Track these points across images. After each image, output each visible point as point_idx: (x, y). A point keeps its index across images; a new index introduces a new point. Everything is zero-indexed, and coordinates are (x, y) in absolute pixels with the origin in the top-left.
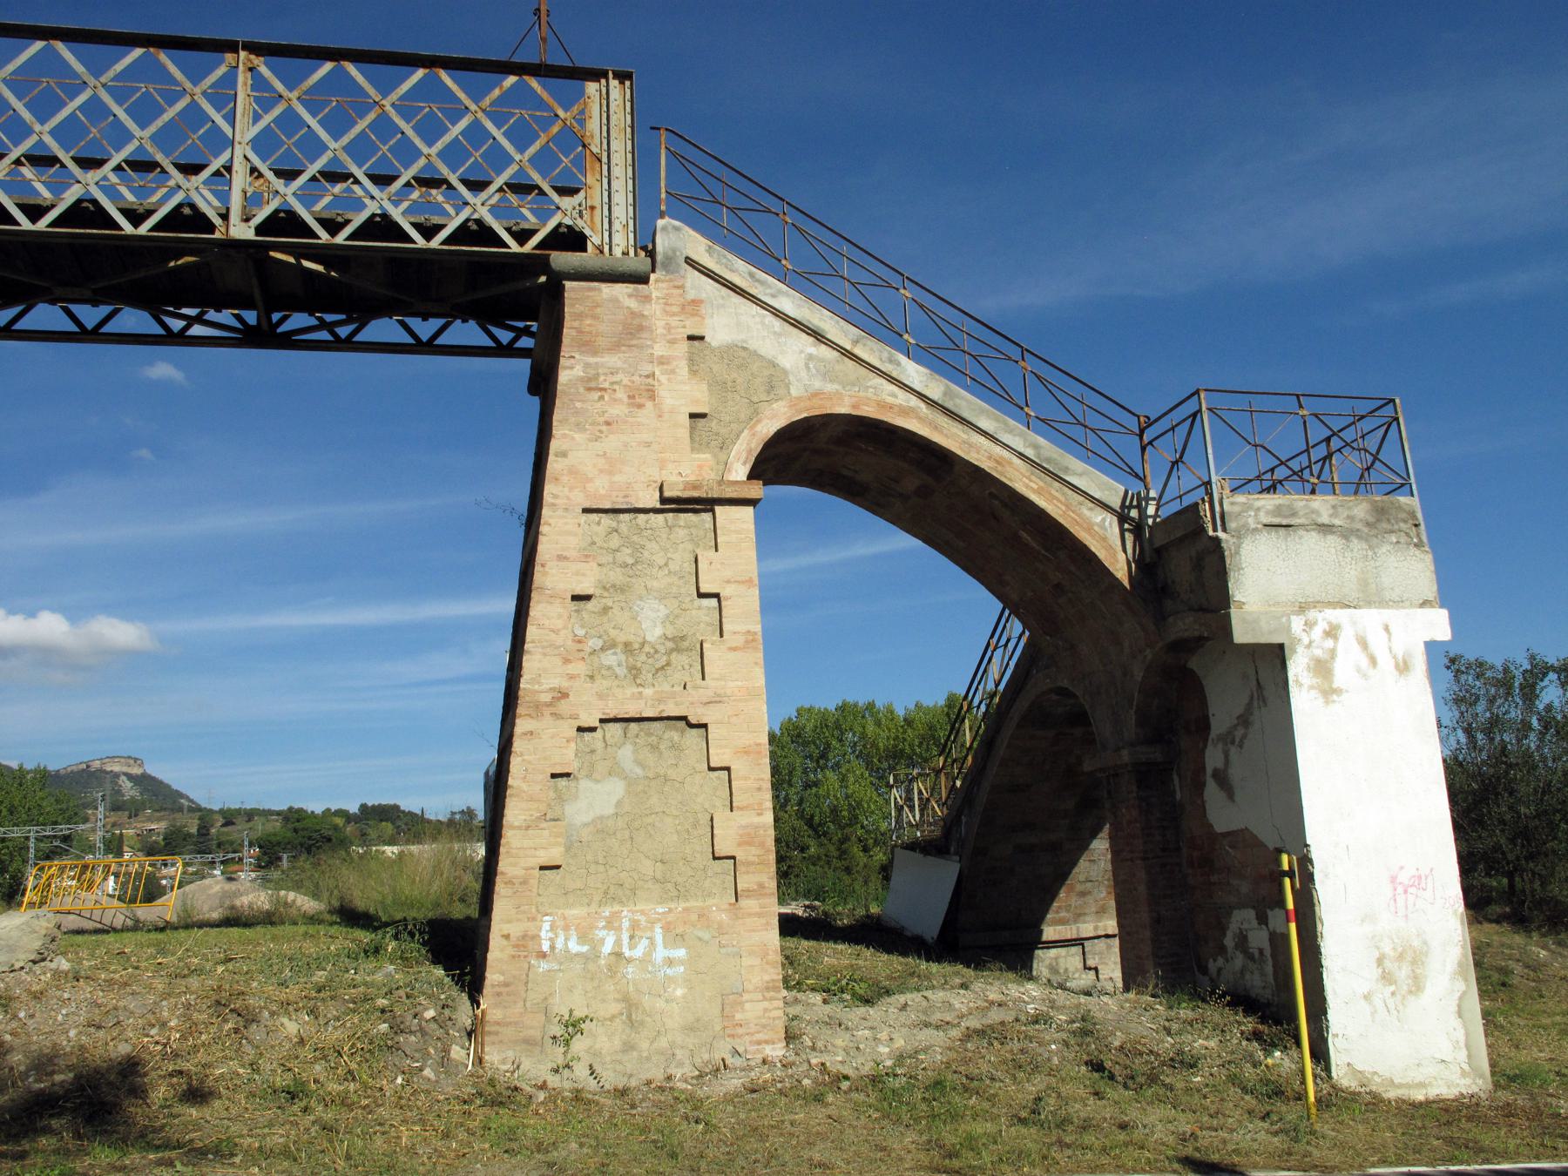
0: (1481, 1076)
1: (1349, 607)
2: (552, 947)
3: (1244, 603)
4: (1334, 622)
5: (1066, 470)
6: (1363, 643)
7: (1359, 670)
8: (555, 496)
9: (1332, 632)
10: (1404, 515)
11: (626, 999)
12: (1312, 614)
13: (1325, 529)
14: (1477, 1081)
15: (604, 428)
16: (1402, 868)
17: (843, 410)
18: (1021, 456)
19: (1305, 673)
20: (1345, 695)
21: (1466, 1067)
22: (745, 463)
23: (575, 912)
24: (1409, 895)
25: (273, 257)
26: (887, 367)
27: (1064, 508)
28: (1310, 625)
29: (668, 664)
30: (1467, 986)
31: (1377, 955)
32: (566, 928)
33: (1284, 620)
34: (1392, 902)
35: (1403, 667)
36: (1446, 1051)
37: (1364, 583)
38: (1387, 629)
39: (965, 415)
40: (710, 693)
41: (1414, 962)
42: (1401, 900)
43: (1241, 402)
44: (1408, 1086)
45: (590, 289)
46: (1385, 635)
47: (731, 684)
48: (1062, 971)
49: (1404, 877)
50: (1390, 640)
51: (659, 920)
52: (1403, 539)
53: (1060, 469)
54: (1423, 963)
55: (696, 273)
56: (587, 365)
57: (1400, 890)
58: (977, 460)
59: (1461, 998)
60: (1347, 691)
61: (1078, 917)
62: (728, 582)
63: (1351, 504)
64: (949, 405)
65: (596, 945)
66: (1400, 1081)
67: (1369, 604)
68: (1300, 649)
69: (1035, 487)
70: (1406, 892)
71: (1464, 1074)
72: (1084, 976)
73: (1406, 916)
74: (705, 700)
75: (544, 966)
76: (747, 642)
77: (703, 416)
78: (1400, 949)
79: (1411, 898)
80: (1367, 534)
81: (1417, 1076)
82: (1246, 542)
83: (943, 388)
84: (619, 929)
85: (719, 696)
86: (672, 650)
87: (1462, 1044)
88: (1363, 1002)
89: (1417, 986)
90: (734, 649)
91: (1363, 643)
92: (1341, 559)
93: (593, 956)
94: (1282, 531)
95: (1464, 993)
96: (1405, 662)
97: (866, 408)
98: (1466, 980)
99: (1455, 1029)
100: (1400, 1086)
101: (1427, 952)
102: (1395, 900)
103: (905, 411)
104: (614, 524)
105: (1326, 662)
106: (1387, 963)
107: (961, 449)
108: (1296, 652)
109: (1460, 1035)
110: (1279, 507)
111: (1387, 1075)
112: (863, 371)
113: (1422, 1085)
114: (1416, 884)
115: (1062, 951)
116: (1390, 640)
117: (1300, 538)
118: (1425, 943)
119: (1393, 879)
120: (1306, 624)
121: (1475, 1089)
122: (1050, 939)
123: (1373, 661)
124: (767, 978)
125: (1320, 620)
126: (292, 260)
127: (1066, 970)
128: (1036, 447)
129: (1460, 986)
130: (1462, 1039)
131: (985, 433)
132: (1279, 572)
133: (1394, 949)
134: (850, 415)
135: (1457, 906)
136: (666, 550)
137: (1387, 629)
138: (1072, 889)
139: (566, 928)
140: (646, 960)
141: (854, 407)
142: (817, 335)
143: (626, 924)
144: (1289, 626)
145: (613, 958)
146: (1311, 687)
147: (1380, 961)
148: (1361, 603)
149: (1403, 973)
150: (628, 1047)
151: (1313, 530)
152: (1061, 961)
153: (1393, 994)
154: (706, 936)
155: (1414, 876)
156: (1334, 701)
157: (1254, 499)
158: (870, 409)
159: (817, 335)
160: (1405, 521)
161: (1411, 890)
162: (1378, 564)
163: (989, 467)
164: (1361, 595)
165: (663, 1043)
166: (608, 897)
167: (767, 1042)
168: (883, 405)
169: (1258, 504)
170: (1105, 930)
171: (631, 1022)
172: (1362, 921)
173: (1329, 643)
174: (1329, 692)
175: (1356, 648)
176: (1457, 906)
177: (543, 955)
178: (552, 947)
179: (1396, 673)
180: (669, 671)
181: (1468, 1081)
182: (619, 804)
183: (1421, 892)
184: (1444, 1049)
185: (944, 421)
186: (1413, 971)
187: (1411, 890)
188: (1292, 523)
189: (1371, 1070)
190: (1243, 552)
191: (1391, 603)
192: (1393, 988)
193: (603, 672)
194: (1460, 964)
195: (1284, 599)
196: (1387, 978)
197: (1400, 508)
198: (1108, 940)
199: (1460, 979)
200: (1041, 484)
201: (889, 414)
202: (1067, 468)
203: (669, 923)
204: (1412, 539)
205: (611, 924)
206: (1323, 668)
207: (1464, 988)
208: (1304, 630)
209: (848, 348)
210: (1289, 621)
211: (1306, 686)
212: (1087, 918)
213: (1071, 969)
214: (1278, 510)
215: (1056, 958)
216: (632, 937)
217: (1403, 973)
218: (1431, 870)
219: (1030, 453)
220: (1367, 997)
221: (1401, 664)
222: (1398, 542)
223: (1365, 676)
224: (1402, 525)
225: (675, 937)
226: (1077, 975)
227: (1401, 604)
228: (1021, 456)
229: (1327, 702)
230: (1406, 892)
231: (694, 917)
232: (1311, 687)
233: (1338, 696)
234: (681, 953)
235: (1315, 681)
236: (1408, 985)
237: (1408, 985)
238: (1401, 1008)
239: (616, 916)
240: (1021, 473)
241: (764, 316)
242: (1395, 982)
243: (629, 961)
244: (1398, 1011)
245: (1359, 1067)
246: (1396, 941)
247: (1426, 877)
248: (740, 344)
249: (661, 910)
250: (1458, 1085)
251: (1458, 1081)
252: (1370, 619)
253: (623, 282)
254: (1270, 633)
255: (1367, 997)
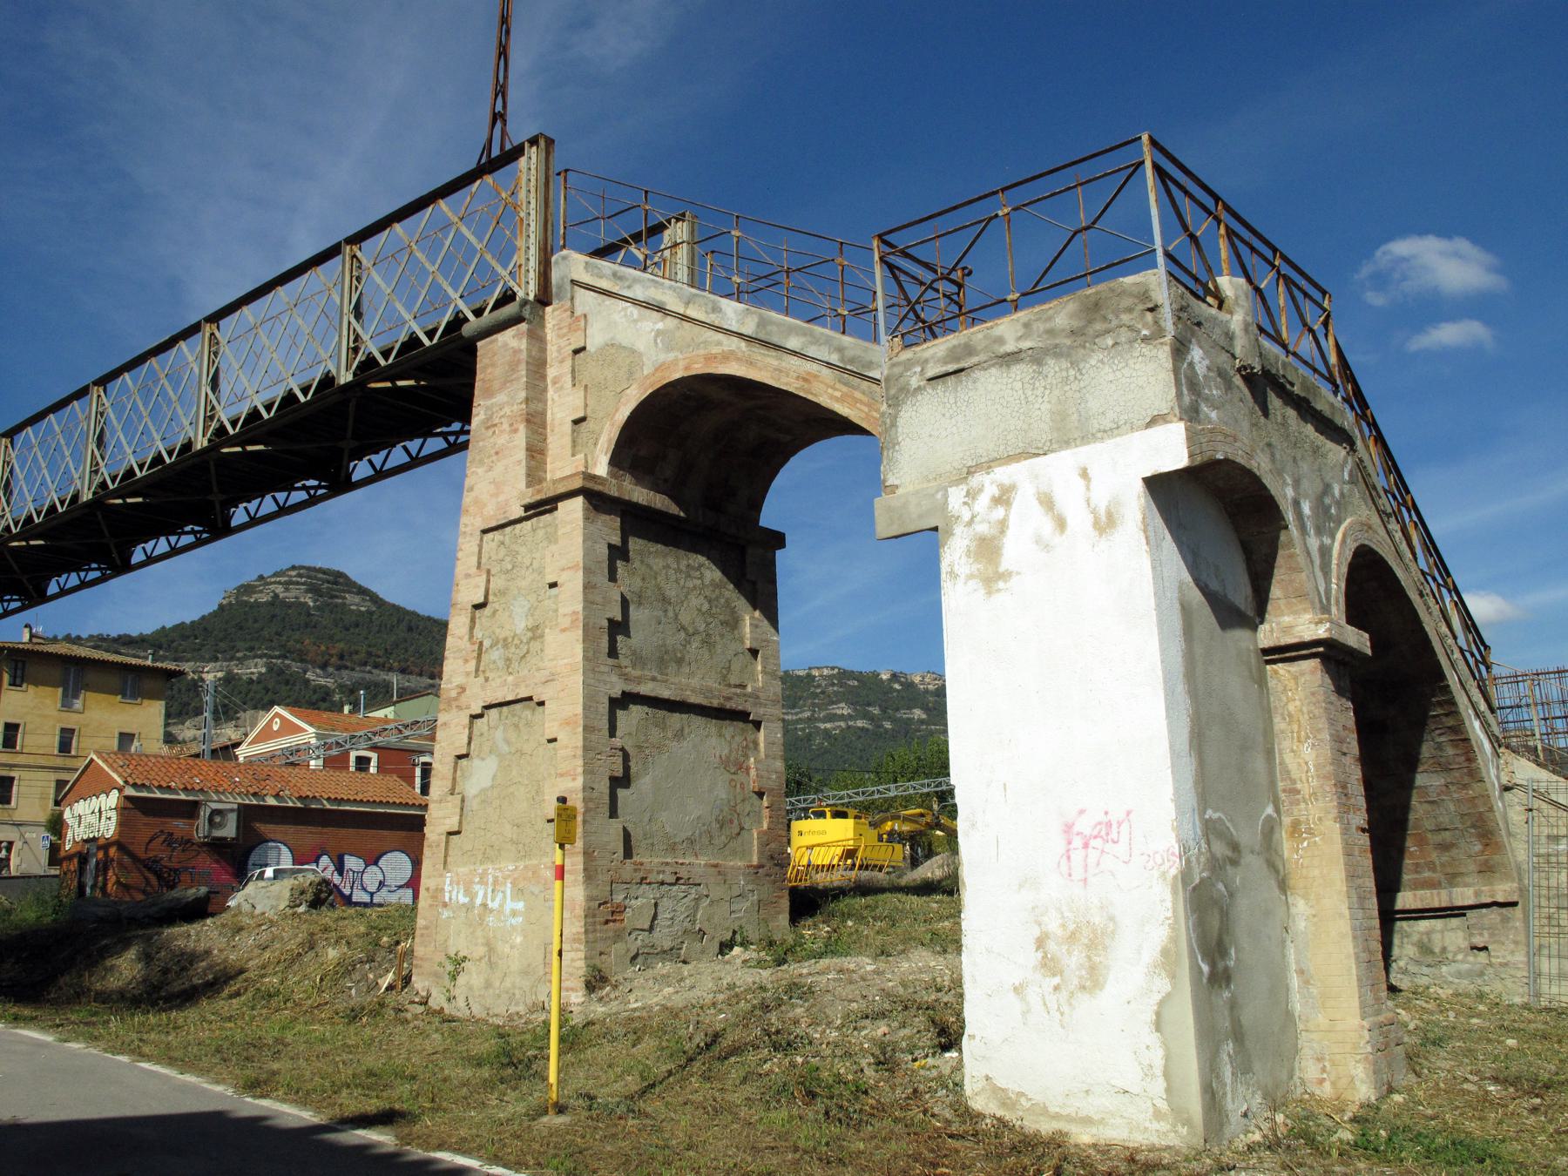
0: (1188, 1122)
1: (1038, 455)
2: (450, 899)
3: (897, 487)
4: (1007, 482)
5: (870, 365)
6: (1047, 502)
7: (1038, 541)
8: (466, 525)
9: (1003, 498)
10: (1127, 302)
11: (488, 944)
12: (975, 481)
13: (1009, 359)
14: (1179, 1128)
15: (494, 458)
16: (1082, 812)
17: (677, 376)
18: (829, 365)
19: (964, 559)
20: (1014, 580)
21: (1163, 1106)
22: (606, 454)
23: (462, 869)
24: (1090, 850)
25: (1218, 243)
26: (712, 318)
27: (866, 410)
28: (972, 495)
29: (528, 652)
30: (1174, 986)
31: (1037, 932)
32: (458, 884)
33: (939, 496)
34: (1064, 860)
35: (1106, 523)
36: (1130, 1077)
37: (1060, 419)
38: (1084, 474)
39: (775, 340)
40: (547, 673)
41: (1092, 946)
42: (1077, 856)
43: (925, 231)
44: (1069, 1119)
45: (491, 342)
46: (1082, 482)
47: (561, 662)
48: (1437, 950)
49: (1084, 825)
50: (1088, 488)
51: (509, 876)
52: (1124, 335)
53: (863, 366)
54: (1105, 948)
55: (583, 290)
56: (487, 408)
57: (1077, 842)
58: (787, 384)
59: (1161, 1003)
60: (1018, 573)
61: (1453, 878)
62: (563, 570)
63: (1051, 312)
64: (762, 336)
65: (473, 897)
66: (1057, 1110)
67: (1066, 443)
68: (959, 530)
69: (838, 394)
70: (1086, 846)
71: (1158, 1115)
72: (1471, 959)
73: (1085, 880)
74: (543, 680)
75: (446, 914)
76: (572, 622)
77: (583, 419)
78: (1072, 927)
79: (1093, 855)
80: (1070, 347)
81: (1089, 1107)
82: (905, 408)
83: (756, 320)
84: (487, 884)
85: (553, 675)
86: (531, 639)
87: (1158, 1071)
88: (1012, 994)
89: (1093, 980)
90: (564, 630)
91: (1047, 502)
92: (1029, 393)
93: (469, 908)
94: (951, 380)
95: (1168, 995)
96: (1110, 515)
97: (696, 366)
98: (1173, 977)
99: (1148, 1047)
100: (1057, 1117)
101: (1113, 932)
102: (1069, 858)
103: (726, 357)
104: (501, 538)
105: (993, 538)
106: (1052, 946)
107: (772, 377)
108: (953, 534)
109: (1157, 1057)
110: (952, 350)
111: (1038, 1098)
112: (697, 329)
113: (1087, 1121)
114: (1103, 833)
115: (1438, 924)
116: (1088, 488)
117: (974, 382)
118: (1112, 919)
119: (1068, 828)
120: (968, 494)
121: (1172, 1140)
122: (1408, 907)
123: (1061, 524)
124: (574, 930)
125: (987, 485)
126: (389, 384)
127: (1444, 950)
128: (840, 350)
129: (1163, 985)
130: (1159, 1063)
131: (794, 353)
132: (944, 434)
133: (1063, 926)
134: (683, 378)
135: (1167, 865)
136: (531, 551)
137: (1084, 474)
138: (1422, 842)
139: (458, 884)
140: (500, 911)
141: (687, 368)
142: (660, 309)
143: (491, 880)
144: (946, 503)
145: (482, 908)
146: (971, 577)
147: (1040, 943)
148: (1055, 446)
149: (1074, 960)
150: (488, 985)
151: (993, 365)
152: (1436, 938)
153: (1056, 988)
154: (536, 890)
155: (1100, 823)
156: (999, 590)
157: (923, 350)
158: (699, 366)
159: (660, 309)
160: (1130, 310)
161: (1093, 843)
162: (1082, 384)
163: (796, 388)
164: (1055, 435)
165: (508, 984)
166: (486, 859)
167: (572, 989)
168: (710, 358)
169: (927, 354)
170: (1492, 896)
171: (491, 964)
172: (1021, 886)
173: (1000, 512)
174: (992, 575)
175: (1037, 509)
176: (1167, 865)
177: (445, 905)
178: (450, 899)
179: (1093, 533)
180: (528, 657)
181: (1164, 1126)
182: (494, 777)
183: (1109, 847)
184: (1130, 1077)
185: (759, 353)
186: (1089, 958)
187: (1093, 843)
188: (966, 365)
189: (1017, 1090)
190: (900, 422)
191: (1099, 435)
192: (1056, 980)
193: (491, 666)
194: (1165, 952)
195: (948, 467)
196: (1049, 965)
197: (1123, 293)
198: (1504, 910)
199: (1164, 974)
200: (845, 389)
201: (714, 365)
202: (871, 362)
203: (515, 879)
204: (1139, 332)
205: (483, 882)
206: (988, 549)
207: (1168, 988)
208: (965, 503)
209: (681, 312)
210: (946, 497)
211: (963, 576)
212: (1469, 880)
213: (1451, 948)
214: (953, 355)
215: (1428, 933)
216: (493, 891)
217: (1074, 960)
218: (1128, 813)
219: (834, 359)
220: (1018, 990)
221: (1104, 518)
222: (1116, 344)
223: (1047, 548)
224: (1125, 318)
225: (519, 893)
226: (1460, 957)
227: (1116, 432)
228: (829, 365)
229: (989, 593)
230: (1086, 846)
231: (530, 874)
232: (971, 577)
233: (1006, 582)
234: (520, 905)
235: (975, 567)
236: (1081, 977)
237: (1081, 977)
238: (1065, 1009)
239: (485, 873)
240: (826, 384)
241: (625, 309)
242: (1061, 973)
243: (491, 911)
244: (1062, 1014)
245: (1001, 1082)
246: (1066, 914)
247: (1119, 824)
248: (610, 343)
249: (510, 868)
250: (1146, 1129)
251: (1147, 1124)
252: (1060, 467)
253: (510, 327)
254: (920, 516)
255: (1018, 990)
